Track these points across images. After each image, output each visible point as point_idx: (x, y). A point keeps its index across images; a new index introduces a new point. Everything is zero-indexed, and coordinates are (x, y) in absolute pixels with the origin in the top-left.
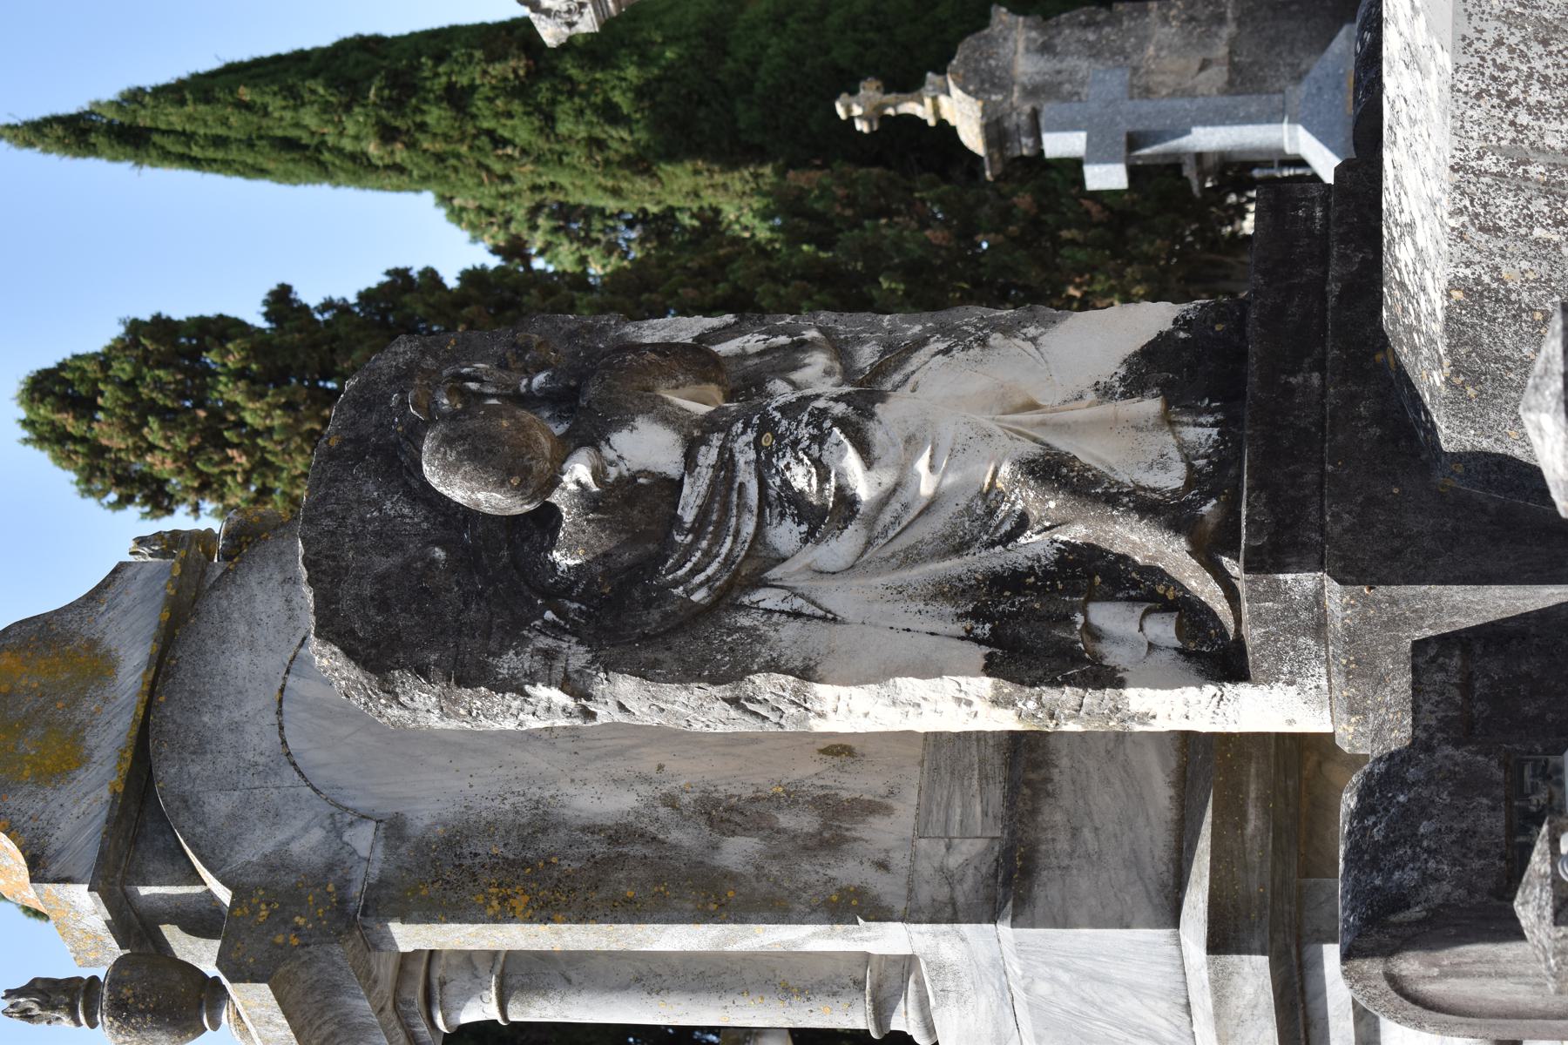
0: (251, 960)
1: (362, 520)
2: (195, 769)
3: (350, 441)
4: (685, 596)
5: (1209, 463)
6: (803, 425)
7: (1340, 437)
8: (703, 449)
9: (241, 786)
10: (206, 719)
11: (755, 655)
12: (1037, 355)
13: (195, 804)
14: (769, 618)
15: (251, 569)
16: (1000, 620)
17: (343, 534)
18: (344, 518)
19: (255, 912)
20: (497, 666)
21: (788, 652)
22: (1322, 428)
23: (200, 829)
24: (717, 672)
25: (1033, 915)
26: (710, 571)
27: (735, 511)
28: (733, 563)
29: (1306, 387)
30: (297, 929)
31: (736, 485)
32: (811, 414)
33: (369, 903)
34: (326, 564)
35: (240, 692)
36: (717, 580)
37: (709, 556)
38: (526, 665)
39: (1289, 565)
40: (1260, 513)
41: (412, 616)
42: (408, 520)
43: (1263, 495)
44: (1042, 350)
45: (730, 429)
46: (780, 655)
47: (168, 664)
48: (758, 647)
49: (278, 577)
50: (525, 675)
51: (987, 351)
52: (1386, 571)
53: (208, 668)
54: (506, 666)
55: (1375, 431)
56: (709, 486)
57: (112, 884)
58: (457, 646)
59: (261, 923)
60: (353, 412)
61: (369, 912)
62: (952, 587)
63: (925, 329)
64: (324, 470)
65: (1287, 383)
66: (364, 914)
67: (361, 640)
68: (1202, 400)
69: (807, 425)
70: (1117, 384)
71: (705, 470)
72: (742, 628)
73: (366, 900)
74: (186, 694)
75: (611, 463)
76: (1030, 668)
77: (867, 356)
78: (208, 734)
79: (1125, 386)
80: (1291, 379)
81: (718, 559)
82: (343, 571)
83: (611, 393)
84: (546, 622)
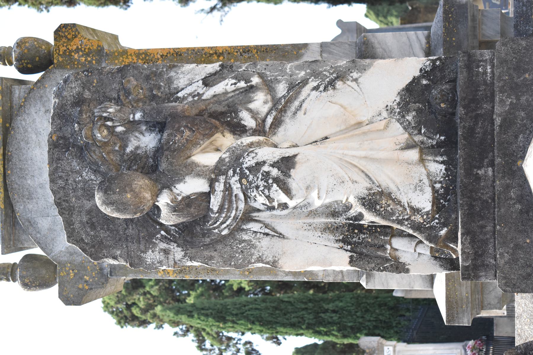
0: (72, 296)
1: (75, 181)
2: (30, 206)
3: (61, 138)
4: (219, 232)
5: (442, 187)
6: (259, 180)
7: (502, 210)
8: (217, 184)
9: (50, 215)
10: (29, 182)
11: (252, 255)
12: (359, 90)
13: (34, 223)
14: (256, 235)
15: (30, 105)
16: (355, 244)
17: (68, 189)
18: (67, 180)
19: (68, 274)
20: (145, 258)
21: (266, 253)
22: (493, 200)
23: (38, 235)
24: (237, 263)
25: (374, 282)
26: (228, 223)
27: (235, 202)
28: (237, 218)
29: (486, 176)
30: (86, 281)
31: (234, 195)
32: (262, 175)
33: (112, 270)
34: (65, 205)
35: (40, 169)
36: (231, 225)
37: (227, 218)
38: (158, 257)
39: (481, 276)
40: (467, 248)
41: (106, 232)
42: (94, 182)
43: (468, 238)
44: (361, 86)
45: (227, 173)
46: (263, 255)
47: (8, 154)
48: (253, 250)
49: (43, 109)
50: (158, 262)
51: (336, 91)
52: (524, 285)
53: (24, 157)
54: (149, 258)
55: (518, 206)
56: (222, 199)
57: (10, 247)
58: (127, 247)
59: (72, 279)
60: (59, 121)
61: (113, 274)
62: (332, 225)
63: (306, 74)
64: (53, 154)
65: (478, 174)
66: (111, 275)
67: (87, 244)
68: (436, 135)
69: (262, 180)
70: (396, 107)
71: (219, 193)
72: (244, 241)
73: (110, 269)
74: (18, 170)
75: (178, 195)
76: (369, 263)
77: (281, 89)
78: (32, 189)
79: (400, 108)
80: (479, 172)
81: (230, 219)
82: (72, 208)
83: (172, 166)
84: (162, 235)
